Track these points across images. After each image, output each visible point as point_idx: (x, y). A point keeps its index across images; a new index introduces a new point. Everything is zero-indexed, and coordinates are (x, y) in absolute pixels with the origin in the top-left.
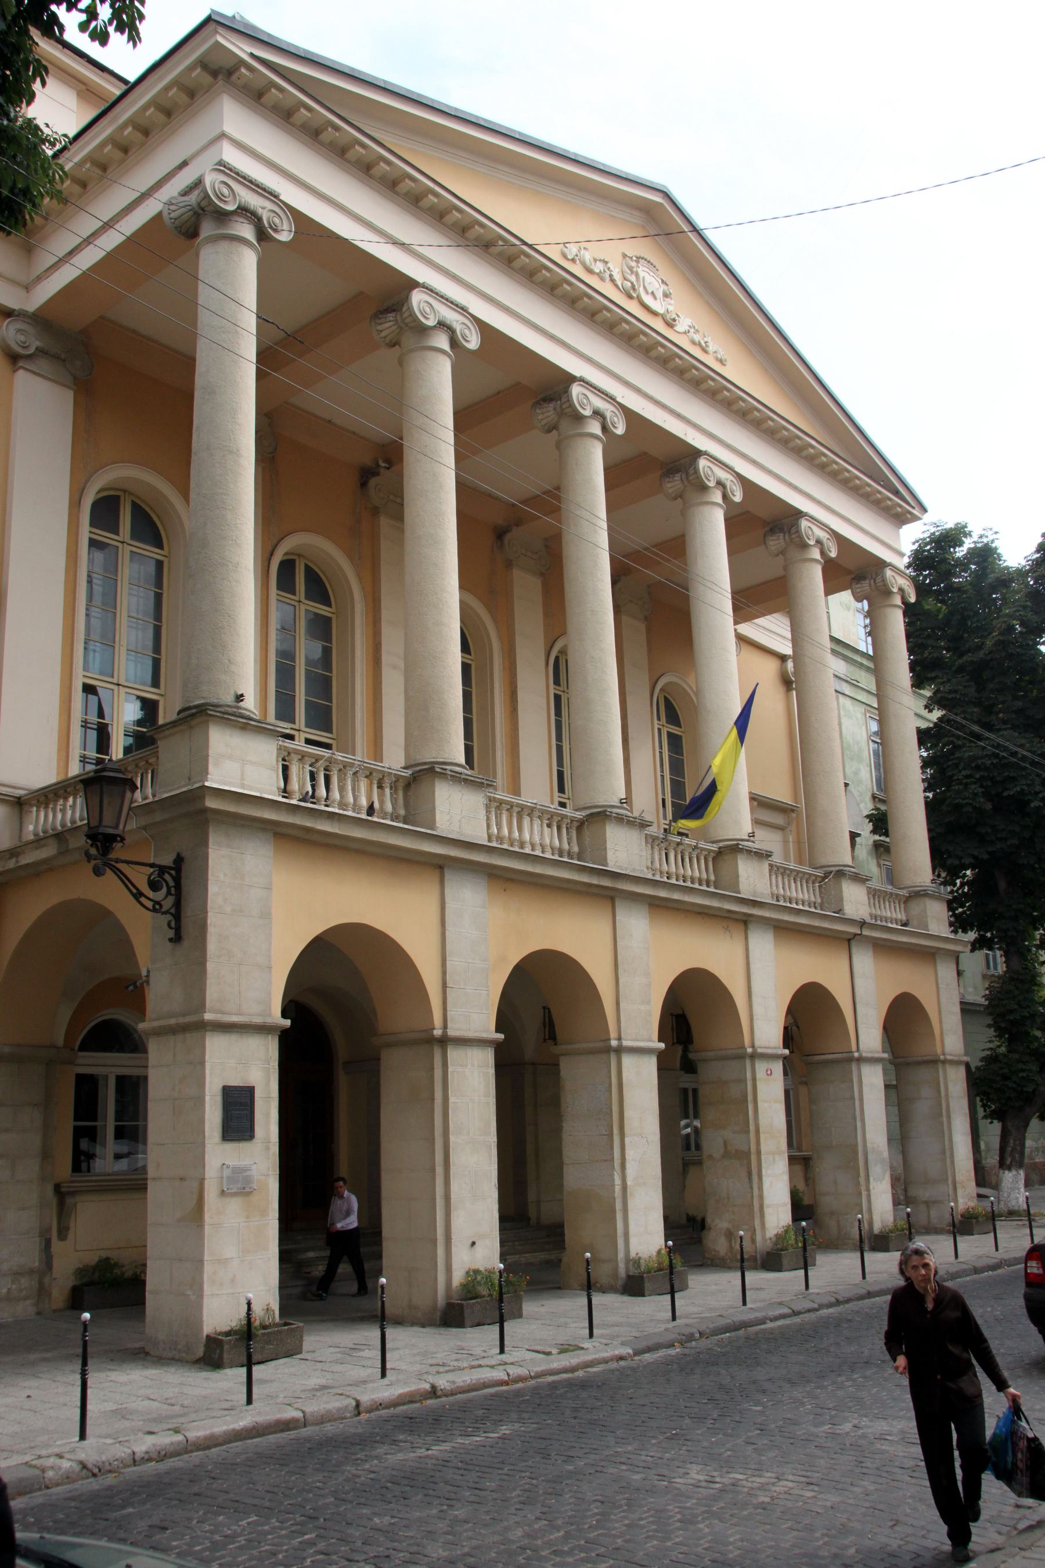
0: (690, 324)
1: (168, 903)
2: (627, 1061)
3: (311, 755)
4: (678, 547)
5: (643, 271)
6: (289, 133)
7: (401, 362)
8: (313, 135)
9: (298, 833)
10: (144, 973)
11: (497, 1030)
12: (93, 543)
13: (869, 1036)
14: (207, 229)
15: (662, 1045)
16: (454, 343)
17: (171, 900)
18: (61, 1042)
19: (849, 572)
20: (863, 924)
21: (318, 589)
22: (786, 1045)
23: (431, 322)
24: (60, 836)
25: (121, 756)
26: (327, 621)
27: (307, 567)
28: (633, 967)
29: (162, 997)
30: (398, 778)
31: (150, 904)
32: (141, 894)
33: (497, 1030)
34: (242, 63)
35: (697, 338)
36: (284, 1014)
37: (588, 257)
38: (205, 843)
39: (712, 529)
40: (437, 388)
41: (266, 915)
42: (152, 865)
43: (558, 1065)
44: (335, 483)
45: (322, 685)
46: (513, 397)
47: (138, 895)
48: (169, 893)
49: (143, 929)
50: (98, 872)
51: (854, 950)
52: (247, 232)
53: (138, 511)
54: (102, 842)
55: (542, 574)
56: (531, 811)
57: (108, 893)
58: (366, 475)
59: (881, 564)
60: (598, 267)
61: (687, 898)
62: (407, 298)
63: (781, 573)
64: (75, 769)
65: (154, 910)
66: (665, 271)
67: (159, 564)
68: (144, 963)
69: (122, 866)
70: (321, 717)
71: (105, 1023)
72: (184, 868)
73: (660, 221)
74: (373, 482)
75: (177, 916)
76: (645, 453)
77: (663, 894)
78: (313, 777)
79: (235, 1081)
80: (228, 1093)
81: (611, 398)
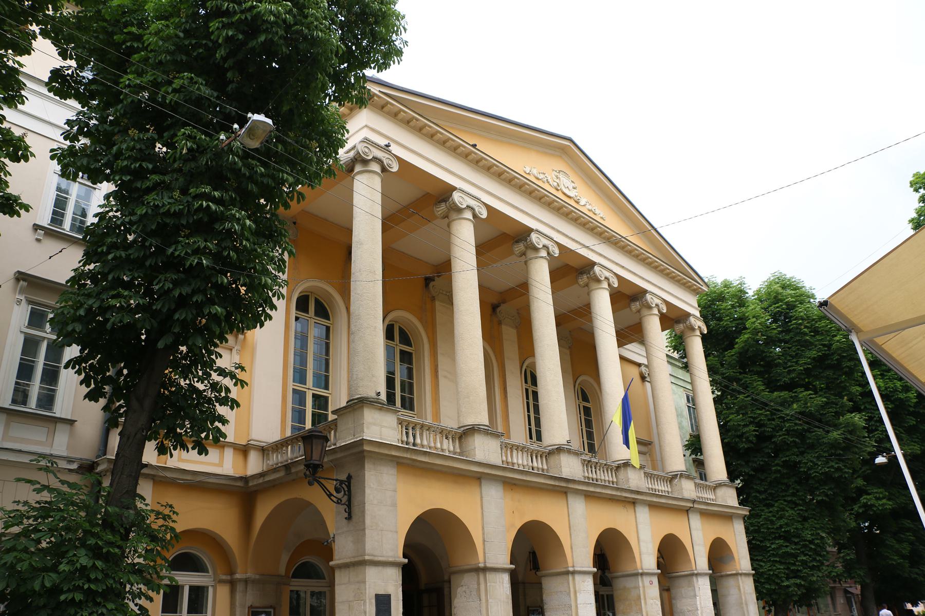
0: (588, 202)
1: (345, 499)
2: (578, 578)
3: (406, 421)
4: (586, 311)
5: (561, 176)
6: (396, 123)
7: (449, 226)
8: (407, 123)
9: (409, 463)
10: (332, 536)
11: (511, 563)
12: (297, 319)
13: (701, 562)
14: (358, 168)
15: (595, 570)
16: (475, 216)
17: (346, 498)
18: (283, 574)
19: (673, 320)
20: (694, 501)
21: (405, 339)
22: (658, 568)
23: (540, 246)
24: (287, 467)
25: (310, 427)
26: (410, 354)
27: (400, 329)
28: (577, 529)
29: (343, 550)
30: (456, 433)
31: (335, 500)
32: (332, 495)
33: (511, 563)
34: (375, 94)
35: (590, 207)
36: (405, 556)
37: (535, 171)
38: (363, 467)
39: (541, 276)
40: (464, 237)
41: (394, 505)
42: (336, 480)
43: (541, 583)
44: (418, 286)
45: (408, 387)
46: (503, 241)
47: (330, 495)
48: (345, 494)
49: (331, 513)
50: (310, 484)
51: (690, 516)
52: (376, 167)
53: (318, 304)
54: (313, 471)
55: (517, 327)
56: (559, 450)
57: (315, 496)
58: (428, 280)
59: (688, 315)
60: (541, 176)
61: (604, 491)
62: (529, 236)
63: (638, 321)
64: (288, 433)
65: (338, 503)
66: (573, 177)
67: (328, 329)
68: (332, 531)
69: (321, 480)
70: (408, 404)
71: (304, 564)
72: (352, 481)
73: (563, 149)
74: (431, 284)
75: (349, 504)
76: (567, 265)
77: (592, 489)
78: (407, 433)
79: (381, 592)
80: (378, 597)
81: (551, 239)
